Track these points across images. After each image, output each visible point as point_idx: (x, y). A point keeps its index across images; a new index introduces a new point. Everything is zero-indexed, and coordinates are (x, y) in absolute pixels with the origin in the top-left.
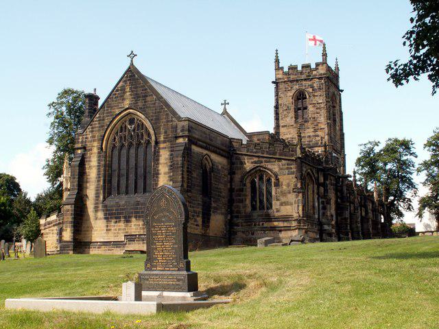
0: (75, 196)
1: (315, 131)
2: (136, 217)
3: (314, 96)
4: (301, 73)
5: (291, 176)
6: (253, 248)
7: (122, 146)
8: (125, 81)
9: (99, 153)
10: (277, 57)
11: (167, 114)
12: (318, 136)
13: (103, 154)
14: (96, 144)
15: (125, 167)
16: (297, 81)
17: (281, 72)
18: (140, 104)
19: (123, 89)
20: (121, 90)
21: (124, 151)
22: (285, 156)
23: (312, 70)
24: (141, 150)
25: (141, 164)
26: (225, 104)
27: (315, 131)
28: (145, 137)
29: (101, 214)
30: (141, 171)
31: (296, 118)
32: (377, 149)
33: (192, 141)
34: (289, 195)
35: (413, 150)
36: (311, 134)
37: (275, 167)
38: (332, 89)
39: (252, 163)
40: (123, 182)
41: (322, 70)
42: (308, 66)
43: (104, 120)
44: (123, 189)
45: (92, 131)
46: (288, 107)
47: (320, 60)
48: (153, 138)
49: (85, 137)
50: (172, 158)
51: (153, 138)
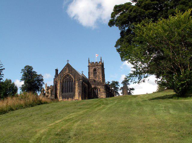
4: (95, 64)
6: (113, 98)
16: (94, 66)
19: (66, 69)
21: (66, 83)
23: (98, 64)
24: (71, 82)
25: (71, 85)
26: (82, 72)
28: (72, 80)
29: (61, 97)
30: (71, 87)
31: (94, 75)
32: (110, 84)
35: (118, 84)
37: (99, 87)
40: (66, 89)
41: (100, 64)
42: (97, 62)
48: (74, 80)
50: (79, 84)
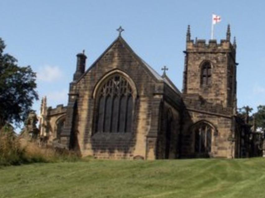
0: (70, 131)
1: (217, 95)
2: (118, 150)
3: (218, 67)
4: (208, 47)
5: (227, 129)
7: (109, 96)
8: (115, 49)
9: (90, 100)
10: (189, 31)
11: (147, 77)
12: (218, 99)
13: (93, 101)
14: (87, 93)
15: (110, 112)
16: (205, 53)
17: (191, 44)
18: (126, 67)
19: (112, 54)
20: (111, 55)
21: (110, 100)
22: (224, 114)
23: (217, 46)
24: (124, 100)
25: (124, 110)
26: (165, 69)
27: (217, 95)
28: (128, 91)
29: (89, 146)
30: (123, 116)
31: (202, 83)
32: (250, 114)
33: (165, 98)
34: (225, 143)
36: (213, 98)
37: (215, 121)
38: (232, 63)
39: (198, 117)
40: (108, 122)
41: (226, 46)
43: (95, 75)
44: (108, 128)
45: (85, 83)
46: (195, 74)
47: (225, 38)
48: (135, 93)
49: (78, 86)
50: (150, 108)
51: (135, 93)
